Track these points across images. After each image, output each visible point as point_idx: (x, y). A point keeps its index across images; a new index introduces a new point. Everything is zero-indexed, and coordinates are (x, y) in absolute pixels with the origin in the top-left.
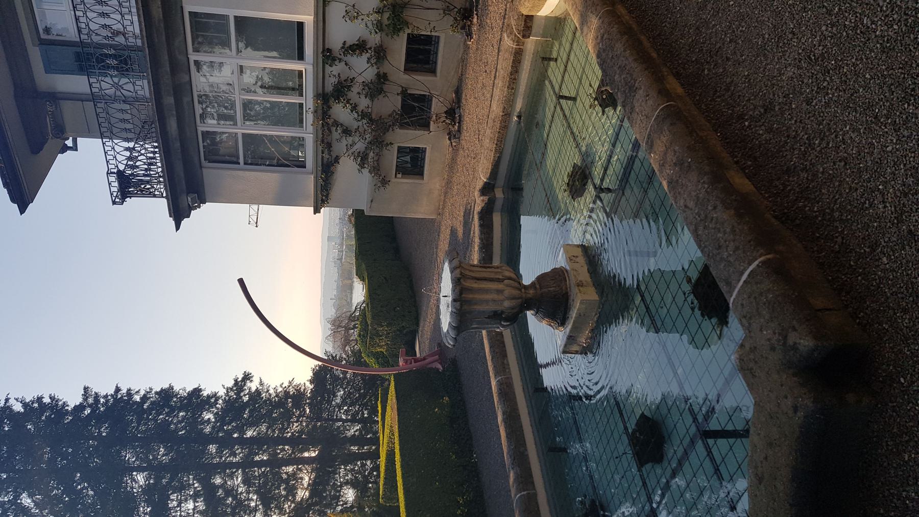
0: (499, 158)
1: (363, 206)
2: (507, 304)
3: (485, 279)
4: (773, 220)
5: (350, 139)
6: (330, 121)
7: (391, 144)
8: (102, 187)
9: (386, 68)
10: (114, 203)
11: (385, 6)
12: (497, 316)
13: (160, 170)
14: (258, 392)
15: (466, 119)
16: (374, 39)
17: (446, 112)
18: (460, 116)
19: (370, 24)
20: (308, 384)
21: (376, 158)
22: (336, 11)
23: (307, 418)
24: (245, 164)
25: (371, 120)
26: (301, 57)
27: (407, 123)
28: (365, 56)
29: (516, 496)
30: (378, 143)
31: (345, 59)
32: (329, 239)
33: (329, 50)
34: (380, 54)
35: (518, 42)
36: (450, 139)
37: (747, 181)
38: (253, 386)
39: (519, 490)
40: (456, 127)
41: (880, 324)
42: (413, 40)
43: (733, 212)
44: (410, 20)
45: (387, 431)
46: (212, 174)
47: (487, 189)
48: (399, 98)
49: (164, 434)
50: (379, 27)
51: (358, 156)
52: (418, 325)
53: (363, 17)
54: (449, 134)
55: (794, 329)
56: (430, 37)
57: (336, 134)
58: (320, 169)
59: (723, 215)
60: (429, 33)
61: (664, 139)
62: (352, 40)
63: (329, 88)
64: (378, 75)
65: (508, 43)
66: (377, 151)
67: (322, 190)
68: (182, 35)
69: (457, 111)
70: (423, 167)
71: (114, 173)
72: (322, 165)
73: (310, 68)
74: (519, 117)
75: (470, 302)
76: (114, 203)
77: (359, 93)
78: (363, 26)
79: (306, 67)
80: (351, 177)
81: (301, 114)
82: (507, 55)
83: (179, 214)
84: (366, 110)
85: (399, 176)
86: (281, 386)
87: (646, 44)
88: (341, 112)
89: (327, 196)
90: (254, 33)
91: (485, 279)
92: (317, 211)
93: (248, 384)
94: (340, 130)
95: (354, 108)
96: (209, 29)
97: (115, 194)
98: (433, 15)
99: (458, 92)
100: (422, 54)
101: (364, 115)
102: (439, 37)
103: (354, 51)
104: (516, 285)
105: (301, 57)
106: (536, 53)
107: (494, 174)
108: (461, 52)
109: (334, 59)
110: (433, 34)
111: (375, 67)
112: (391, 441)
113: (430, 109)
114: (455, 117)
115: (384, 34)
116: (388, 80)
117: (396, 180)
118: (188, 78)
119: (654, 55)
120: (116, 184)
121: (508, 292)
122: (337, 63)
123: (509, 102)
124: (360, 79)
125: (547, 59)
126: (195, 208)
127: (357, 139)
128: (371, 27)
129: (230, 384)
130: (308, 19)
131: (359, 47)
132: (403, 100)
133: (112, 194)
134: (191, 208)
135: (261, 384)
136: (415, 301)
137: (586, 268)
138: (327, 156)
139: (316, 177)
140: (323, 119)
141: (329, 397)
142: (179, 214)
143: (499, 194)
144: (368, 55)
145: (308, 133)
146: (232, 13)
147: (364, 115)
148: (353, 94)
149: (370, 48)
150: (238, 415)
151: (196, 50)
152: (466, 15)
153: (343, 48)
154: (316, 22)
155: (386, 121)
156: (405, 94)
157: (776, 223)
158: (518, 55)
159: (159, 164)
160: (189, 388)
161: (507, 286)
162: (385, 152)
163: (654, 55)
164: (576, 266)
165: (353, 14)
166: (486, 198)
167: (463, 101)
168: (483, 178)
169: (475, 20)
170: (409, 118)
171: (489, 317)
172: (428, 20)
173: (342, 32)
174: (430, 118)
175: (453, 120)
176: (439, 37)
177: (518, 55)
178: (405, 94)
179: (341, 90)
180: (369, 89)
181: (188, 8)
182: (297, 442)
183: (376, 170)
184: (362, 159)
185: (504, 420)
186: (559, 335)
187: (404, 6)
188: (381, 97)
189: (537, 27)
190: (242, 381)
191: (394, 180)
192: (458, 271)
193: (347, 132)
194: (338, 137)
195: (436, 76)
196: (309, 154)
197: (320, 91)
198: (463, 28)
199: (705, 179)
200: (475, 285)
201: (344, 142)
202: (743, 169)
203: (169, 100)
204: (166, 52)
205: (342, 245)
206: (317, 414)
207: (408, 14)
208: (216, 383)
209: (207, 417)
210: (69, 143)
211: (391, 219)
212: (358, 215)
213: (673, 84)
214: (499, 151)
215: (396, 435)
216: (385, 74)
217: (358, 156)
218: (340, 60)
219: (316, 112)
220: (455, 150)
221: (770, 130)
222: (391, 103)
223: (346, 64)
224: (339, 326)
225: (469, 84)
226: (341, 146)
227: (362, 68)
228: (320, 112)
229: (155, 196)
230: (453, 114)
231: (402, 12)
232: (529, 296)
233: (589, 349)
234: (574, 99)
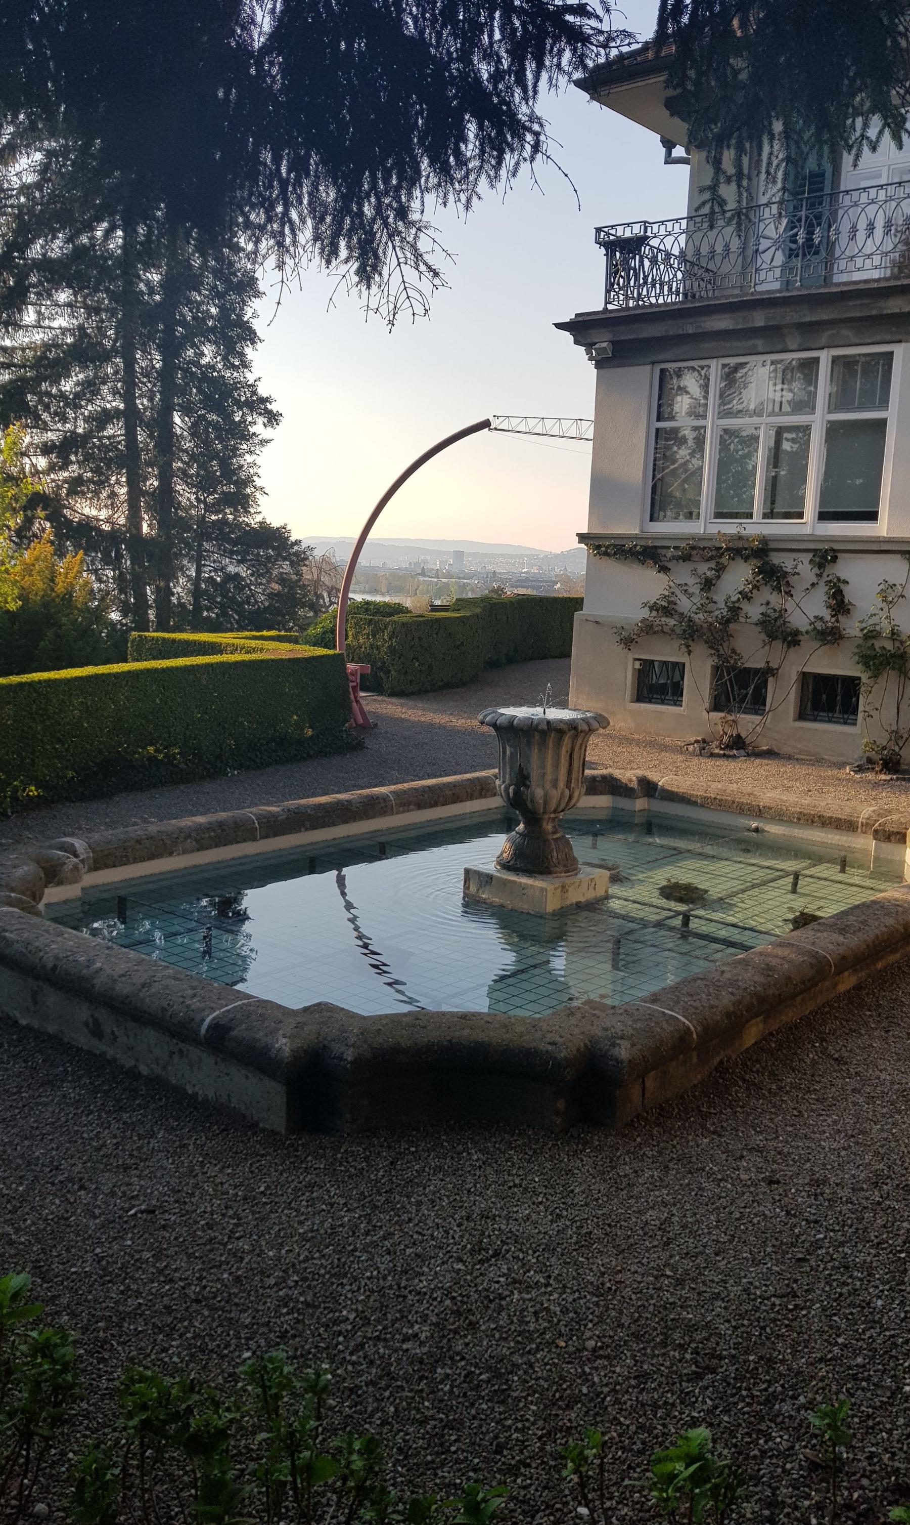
0: (695, 803)
1: (587, 610)
2: (539, 793)
3: (571, 764)
4: (718, 1059)
5: (695, 589)
6: (724, 560)
7: (689, 652)
8: (624, 216)
9: (808, 645)
10: (599, 230)
11: (902, 643)
12: (522, 779)
13: (653, 300)
14: (247, 437)
15: (732, 765)
16: (852, 627)
17: (739, 736)
18: (734, 756)
19: (874, 620)
20: (259, 518)
21: (666, 629)
22: (895, 570)
23: (204, 517)
24: (657, 430)
25: (728, 621)
26: (824, 516)
27: (721, 676)
28: (826, 614)
29: (252, 812)
30: (691, 633)
31: (822, 583)
32: (459, 555)
33: (835, 559)
34: (829, 636)
35: (867, 825)
36: (697, 741)
37: (753, 1042)
38: (259, 428)
39: (259, 817)
40: (717, 751)
41: (639, 1136)
42: (851, 686)
43: (732, 1009)
44: (882, 680)
45: (253, 643)
46: (642, 377)
47: (648, 788)
48: (761, 665)
49: (179, 283)
50: (871, 635)
51: (669, 602)
52: (393, 694)
53: (886, 609)
54: (704, 741)
55: (633, 1045)
56: (855, 711)
57: (705, 569)
58: (650, 543)
59: (726, 1000)
60: (861, 708)
61: (793, 956)
62: (850, 594)
63: (776, 559)
64: (797, 633)
65: (866, 811)
66: (678, 631)
67: (615, 546)
68: (858, 341)
69: (742, 752)
70: (650, 702)
71: (646, 231)
72: (656, 547)
73: (807, 530)
74: (757, 830)
75: (543, 744)
76: (599, 230)
77: (768, 603)
78: (872, 610)
79: (809, 525)
80: (635, 592)
81: (736, 515)
82: (847, 810)
83: (581, 328)
84: (742, 614)
85: (637, 665)
86: (256, 474)
87: (892, 958)
88: (739, 576)
89: (606, 554)
90: (858, 447)
91: (571, 764)
92: (582, 538)
93: (260, 420)
94: (709, 574)
95: (746, 596)
96: (866, 380)
97: (613, 232)
98: (888, 714)
99: (770, 754)
100: (829, 699)
101: (734, 610)
102: (855, 724)
103: (834, 596)
104: (562, 806)
105: (824, 516)
106: (851, 850)
107: (670, 796)
108: (831, 758)
109: (821, 566)
110: (860, 716)
111: (810, 628)
112: (235, 649)
113: (744, 713)
114: (732, 748)
115: (861, 641)
116: (789, 647)
117: (631, 661)
118: (792, 347)
119: (880, 965)
120: (628, 234)
121: (555, 794)
122: (816, 570)
123: (779, 816)
124: (790, 605)
125: (844, 865)
126: (588, 352)
127: (696, 599)
128: (871, 622)
129: (263, 391)
130: (882, 528)
131: (840, 604)
132: (756, 671)
133: (612, 227)
134: (589, 346)
135: (264, 442)
136: (426, 692)
137: (583, 900)
138: (669, 555)
139: (636, 537)
140: (728, 549)
141: (237, 553)
142: (581, 328)
143: (640, 804)
144: (827, 617)
145: (705, 526)
146: (891, 414)
147: (734, 610)
148: (770, 595)
149: (837, 621)
150: (210, 403)
151: (835, 360)
152: (891, 764)
153: (839, 580)
154: (877, 540)
155: (725, 645)
156: (769, 672)
157: (717, 1060)
158: (848, 825)
159: (661, 301)
160: (256, 325)
161: (562, 794)
162: (677, 643)
163: (880, 965)
164: (585, 886)
165: (890, 594)
166: (634, 785)
167: (758, 761)
168: (663, 780)
169: (883, 777)
170: (730, 680)
171: (521, 769)
172: (879, 711)
173: (863, 579)
174: (730, 712)
175: (728, 747)
176: (855, 724)
177: (848, 825)
178: (769, 672)
179: (773, 577)
180: (776, 619)
181: (899, 351)
182: (164, 499)
183: (648, 629)
184: (666, 608)
185: (339, 803)
186: (490, 867)
187: (902, 671)
188: (763, 636)
189: (889, 849)
190: (266, 409)
191: (631, 656)
192: (586, 728)
193: (708, 585)
194: (700, 572)
195: (795, 720)
196: (672, 527)
197: (772, 545)
198: (870, 761)
199: (759, 988)
200: (564, 750)
201: (691, 580)
202: (764, 1039)
203: (759, 319)
204: (833, 316)
205: (449, 575)
206: (205, 531)
207: (890, 677)
208: (267, 367)
209: (206, 352)
210: (679, 151)
211: (566, 654)
212: (577, 603)
213: (847, 982)
214: (704, 803)
215: (247, 657)
216: (796, 643)
217: (669, 602)
218: (819, 576)
219: (740, 538)
220: (680, 750)
221: (814, 1063)
222: (753, 651)
223: (813, 585)
224: (320, 569)
225: (788, 768)
226: (686, 576)
227: (807, 608)
228: (740, 545)
229: (608, 291)
230: (737, 746)
231: (894, 669)
232: (544, 825)
233: (473, 905)
234: (794, 891)
